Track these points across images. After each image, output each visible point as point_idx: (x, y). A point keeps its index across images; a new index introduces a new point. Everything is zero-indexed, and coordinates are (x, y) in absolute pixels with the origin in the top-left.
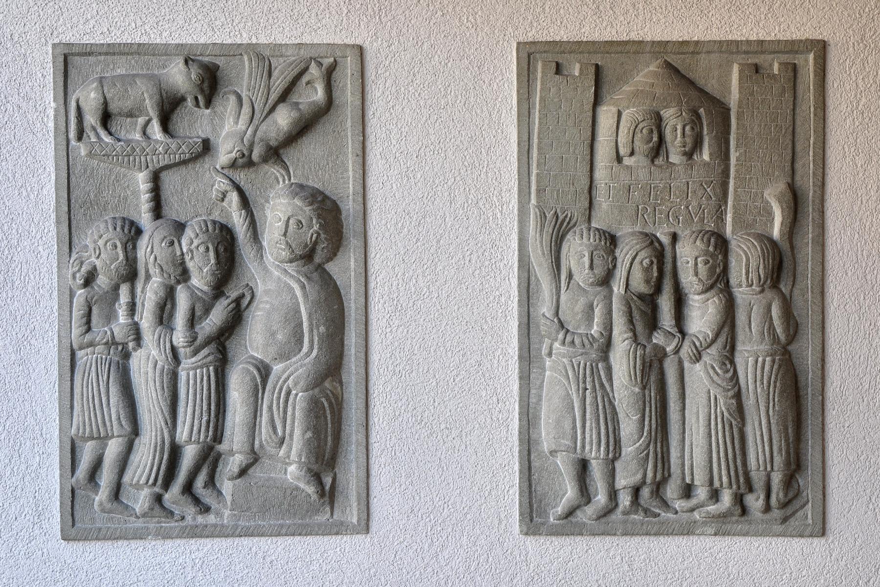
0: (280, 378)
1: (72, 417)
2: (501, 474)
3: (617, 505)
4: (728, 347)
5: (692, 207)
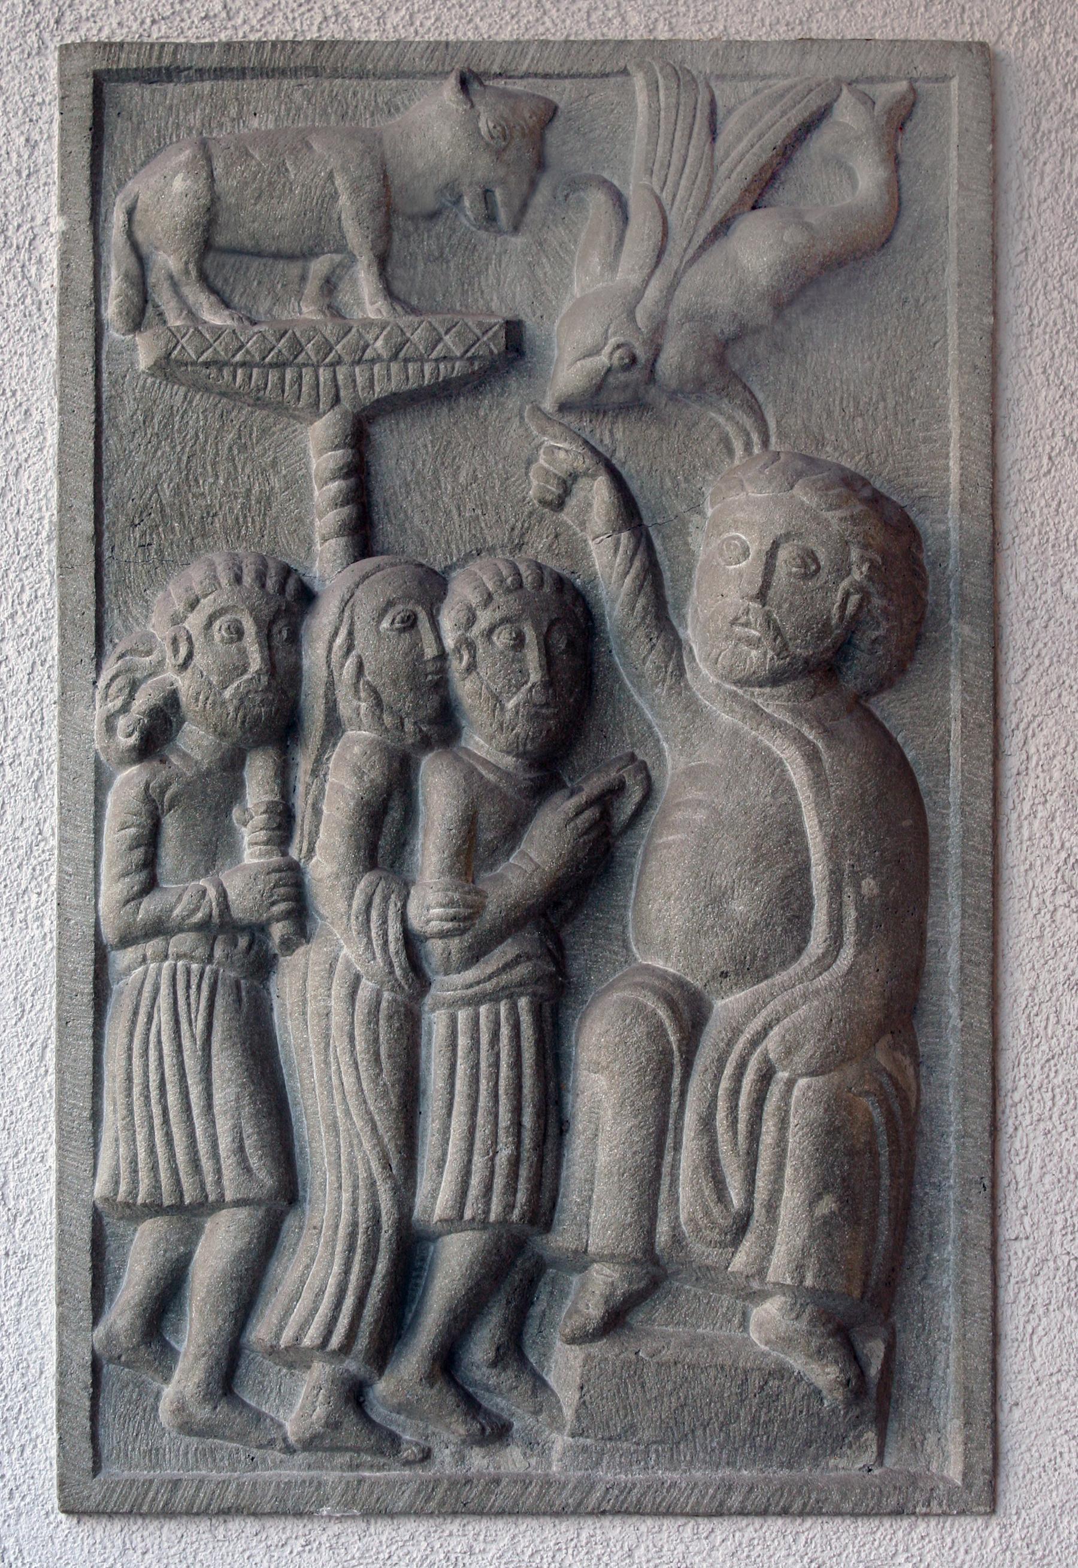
0: (737, 1032)
1: (96, 1145)
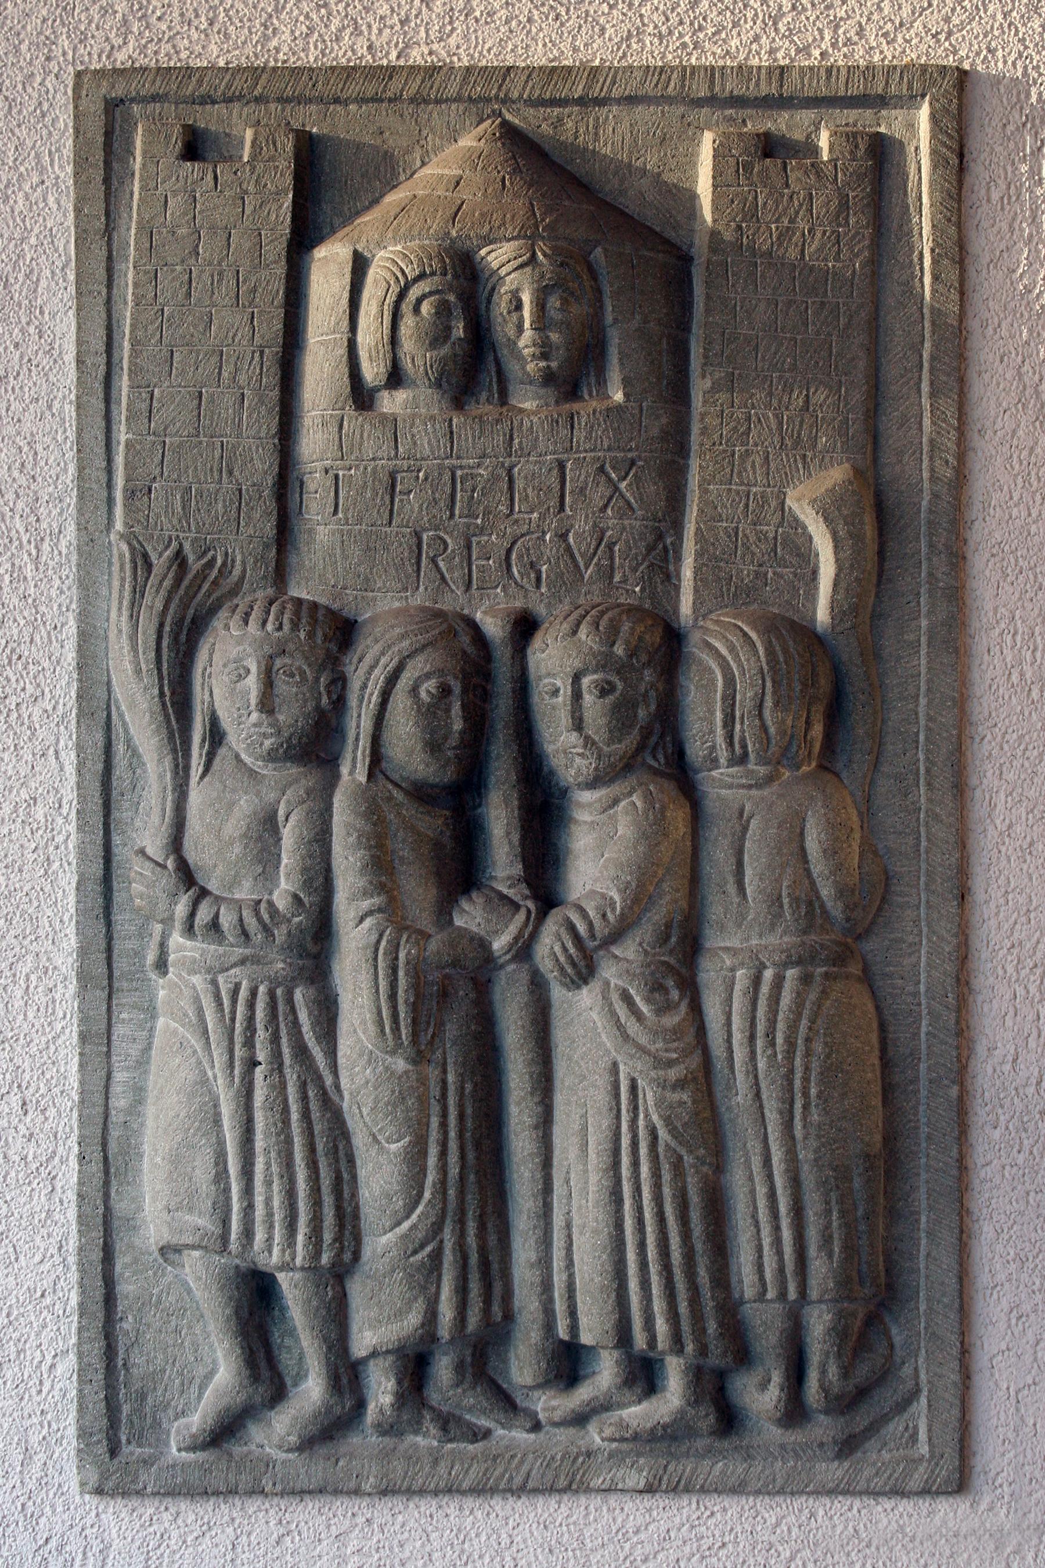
2: (33, 1318)
3: (361, 1405)
4: (673, 940)
5: (576, 534)
